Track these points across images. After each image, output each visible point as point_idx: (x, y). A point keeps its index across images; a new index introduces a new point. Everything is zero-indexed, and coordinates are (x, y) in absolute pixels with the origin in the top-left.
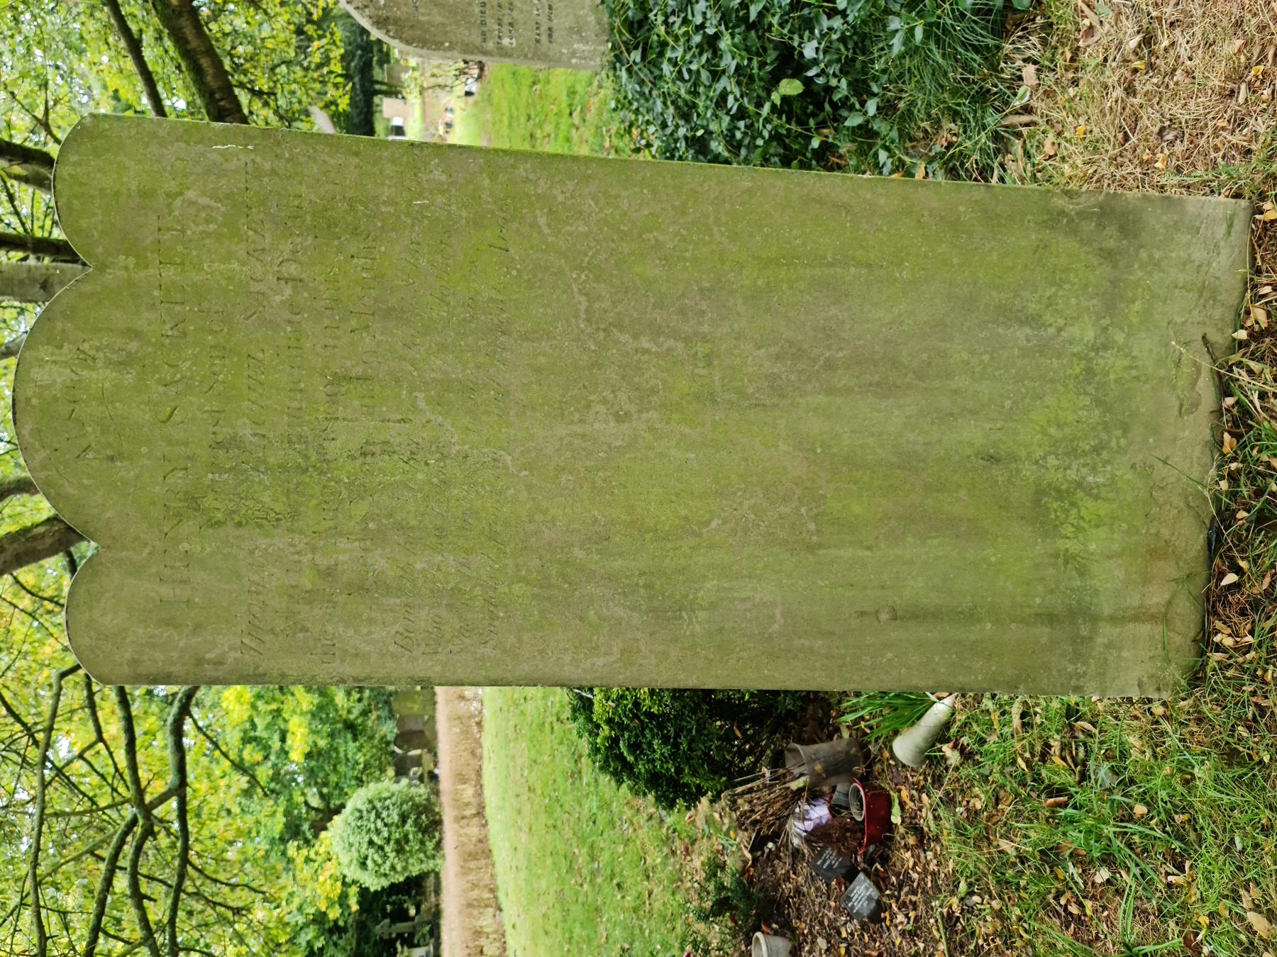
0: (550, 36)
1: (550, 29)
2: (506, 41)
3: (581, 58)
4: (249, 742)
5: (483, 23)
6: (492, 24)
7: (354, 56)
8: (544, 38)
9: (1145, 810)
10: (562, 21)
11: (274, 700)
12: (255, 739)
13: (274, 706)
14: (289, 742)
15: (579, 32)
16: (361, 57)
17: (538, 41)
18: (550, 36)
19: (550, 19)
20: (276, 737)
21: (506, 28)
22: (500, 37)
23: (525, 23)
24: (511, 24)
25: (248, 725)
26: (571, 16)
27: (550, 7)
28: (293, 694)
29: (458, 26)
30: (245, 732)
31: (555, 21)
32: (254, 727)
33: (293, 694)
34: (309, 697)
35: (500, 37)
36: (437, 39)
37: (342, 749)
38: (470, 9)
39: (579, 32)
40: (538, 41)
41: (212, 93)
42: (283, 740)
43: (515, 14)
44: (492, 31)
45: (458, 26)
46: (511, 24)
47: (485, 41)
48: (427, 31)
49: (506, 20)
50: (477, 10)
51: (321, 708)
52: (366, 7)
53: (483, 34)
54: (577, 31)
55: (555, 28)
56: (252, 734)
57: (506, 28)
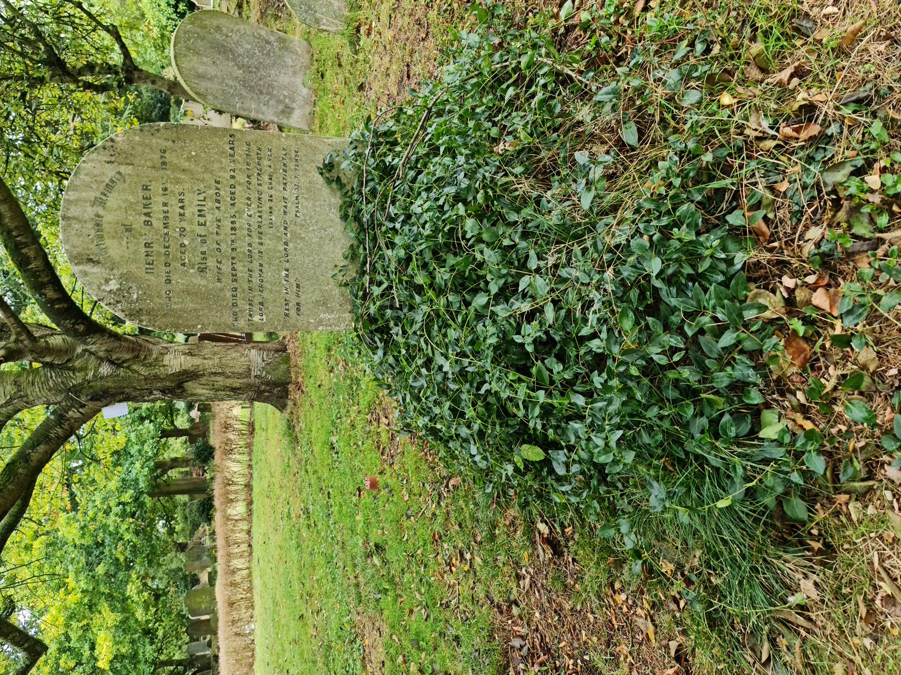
0: (298, 310)
1: (298, 304)
2: (256, 318)
3: (327, 325)
4: (65, 652)
5: (235, 305)
6: (243, 305)
7: (155, 107)
8: (293, 313)
9: (577, 155)
10: (308, 297)
11: (84, 617)
12: (69, 649)
13: (85, 622)
14: (96, 652)
15: (325, 304)
16: (160, 108)
17: (287, 315)
18: (298, 310)
19: (298, 296)
20: (87, 647)
21: (256, 308)
22: (251, 315)
23: (274, 301)
24: (261, 304)
25: (63, 638)
26: (317, 292)
27: (298, 286)
28: (100, 612)
29: (210, 309)
30: (61, 643)
31: (303, 297)
32: (68, 639)
33: (100, 612)
34: (113, 616)
35: (251, 315)
36: (190, 323)
37: (141, 651)
38: (222, 294)
39: (325, 304)
40: (287, 315)
41: (9, 232)
42: (93, 648)
43: (265, 294)
44: (242, 311)
45: (210, 309)
46: (261, 304)
47: (236, 320)
48: (180, 317)
49: (257, 300)
50: (229, 294)
51: (123, 622)
52: (118, 302)
53: (235, 314)
54: (324, 303)
55: (303, 302)
56: (67, 644)
57: (256, 308)
